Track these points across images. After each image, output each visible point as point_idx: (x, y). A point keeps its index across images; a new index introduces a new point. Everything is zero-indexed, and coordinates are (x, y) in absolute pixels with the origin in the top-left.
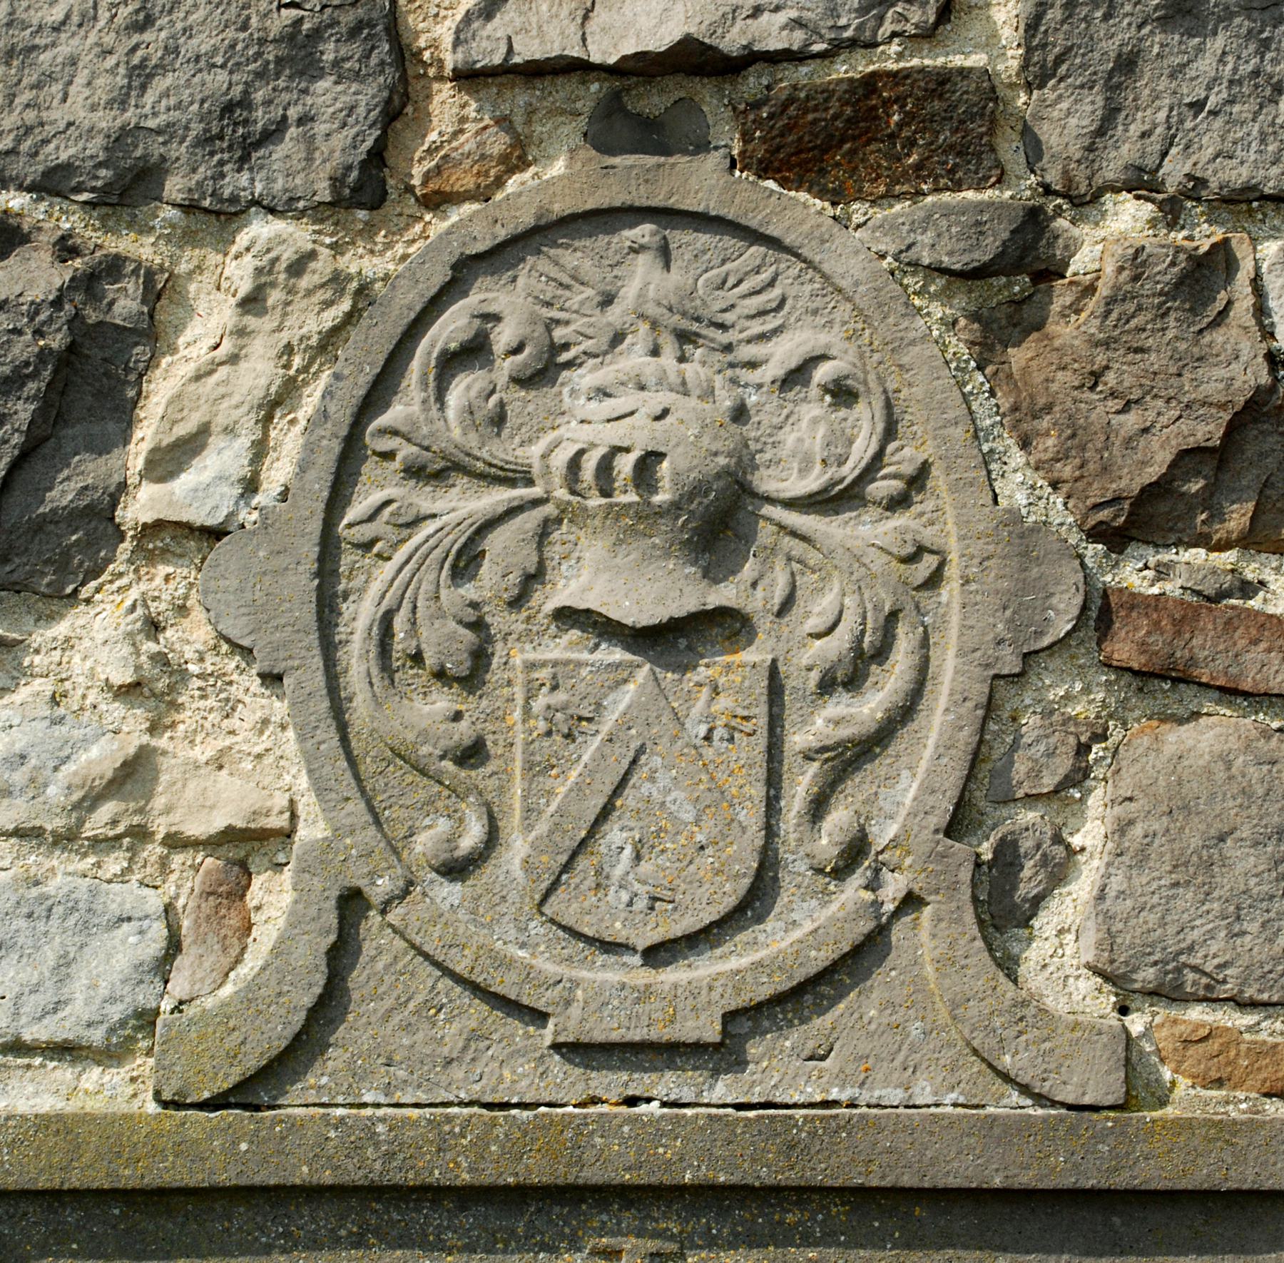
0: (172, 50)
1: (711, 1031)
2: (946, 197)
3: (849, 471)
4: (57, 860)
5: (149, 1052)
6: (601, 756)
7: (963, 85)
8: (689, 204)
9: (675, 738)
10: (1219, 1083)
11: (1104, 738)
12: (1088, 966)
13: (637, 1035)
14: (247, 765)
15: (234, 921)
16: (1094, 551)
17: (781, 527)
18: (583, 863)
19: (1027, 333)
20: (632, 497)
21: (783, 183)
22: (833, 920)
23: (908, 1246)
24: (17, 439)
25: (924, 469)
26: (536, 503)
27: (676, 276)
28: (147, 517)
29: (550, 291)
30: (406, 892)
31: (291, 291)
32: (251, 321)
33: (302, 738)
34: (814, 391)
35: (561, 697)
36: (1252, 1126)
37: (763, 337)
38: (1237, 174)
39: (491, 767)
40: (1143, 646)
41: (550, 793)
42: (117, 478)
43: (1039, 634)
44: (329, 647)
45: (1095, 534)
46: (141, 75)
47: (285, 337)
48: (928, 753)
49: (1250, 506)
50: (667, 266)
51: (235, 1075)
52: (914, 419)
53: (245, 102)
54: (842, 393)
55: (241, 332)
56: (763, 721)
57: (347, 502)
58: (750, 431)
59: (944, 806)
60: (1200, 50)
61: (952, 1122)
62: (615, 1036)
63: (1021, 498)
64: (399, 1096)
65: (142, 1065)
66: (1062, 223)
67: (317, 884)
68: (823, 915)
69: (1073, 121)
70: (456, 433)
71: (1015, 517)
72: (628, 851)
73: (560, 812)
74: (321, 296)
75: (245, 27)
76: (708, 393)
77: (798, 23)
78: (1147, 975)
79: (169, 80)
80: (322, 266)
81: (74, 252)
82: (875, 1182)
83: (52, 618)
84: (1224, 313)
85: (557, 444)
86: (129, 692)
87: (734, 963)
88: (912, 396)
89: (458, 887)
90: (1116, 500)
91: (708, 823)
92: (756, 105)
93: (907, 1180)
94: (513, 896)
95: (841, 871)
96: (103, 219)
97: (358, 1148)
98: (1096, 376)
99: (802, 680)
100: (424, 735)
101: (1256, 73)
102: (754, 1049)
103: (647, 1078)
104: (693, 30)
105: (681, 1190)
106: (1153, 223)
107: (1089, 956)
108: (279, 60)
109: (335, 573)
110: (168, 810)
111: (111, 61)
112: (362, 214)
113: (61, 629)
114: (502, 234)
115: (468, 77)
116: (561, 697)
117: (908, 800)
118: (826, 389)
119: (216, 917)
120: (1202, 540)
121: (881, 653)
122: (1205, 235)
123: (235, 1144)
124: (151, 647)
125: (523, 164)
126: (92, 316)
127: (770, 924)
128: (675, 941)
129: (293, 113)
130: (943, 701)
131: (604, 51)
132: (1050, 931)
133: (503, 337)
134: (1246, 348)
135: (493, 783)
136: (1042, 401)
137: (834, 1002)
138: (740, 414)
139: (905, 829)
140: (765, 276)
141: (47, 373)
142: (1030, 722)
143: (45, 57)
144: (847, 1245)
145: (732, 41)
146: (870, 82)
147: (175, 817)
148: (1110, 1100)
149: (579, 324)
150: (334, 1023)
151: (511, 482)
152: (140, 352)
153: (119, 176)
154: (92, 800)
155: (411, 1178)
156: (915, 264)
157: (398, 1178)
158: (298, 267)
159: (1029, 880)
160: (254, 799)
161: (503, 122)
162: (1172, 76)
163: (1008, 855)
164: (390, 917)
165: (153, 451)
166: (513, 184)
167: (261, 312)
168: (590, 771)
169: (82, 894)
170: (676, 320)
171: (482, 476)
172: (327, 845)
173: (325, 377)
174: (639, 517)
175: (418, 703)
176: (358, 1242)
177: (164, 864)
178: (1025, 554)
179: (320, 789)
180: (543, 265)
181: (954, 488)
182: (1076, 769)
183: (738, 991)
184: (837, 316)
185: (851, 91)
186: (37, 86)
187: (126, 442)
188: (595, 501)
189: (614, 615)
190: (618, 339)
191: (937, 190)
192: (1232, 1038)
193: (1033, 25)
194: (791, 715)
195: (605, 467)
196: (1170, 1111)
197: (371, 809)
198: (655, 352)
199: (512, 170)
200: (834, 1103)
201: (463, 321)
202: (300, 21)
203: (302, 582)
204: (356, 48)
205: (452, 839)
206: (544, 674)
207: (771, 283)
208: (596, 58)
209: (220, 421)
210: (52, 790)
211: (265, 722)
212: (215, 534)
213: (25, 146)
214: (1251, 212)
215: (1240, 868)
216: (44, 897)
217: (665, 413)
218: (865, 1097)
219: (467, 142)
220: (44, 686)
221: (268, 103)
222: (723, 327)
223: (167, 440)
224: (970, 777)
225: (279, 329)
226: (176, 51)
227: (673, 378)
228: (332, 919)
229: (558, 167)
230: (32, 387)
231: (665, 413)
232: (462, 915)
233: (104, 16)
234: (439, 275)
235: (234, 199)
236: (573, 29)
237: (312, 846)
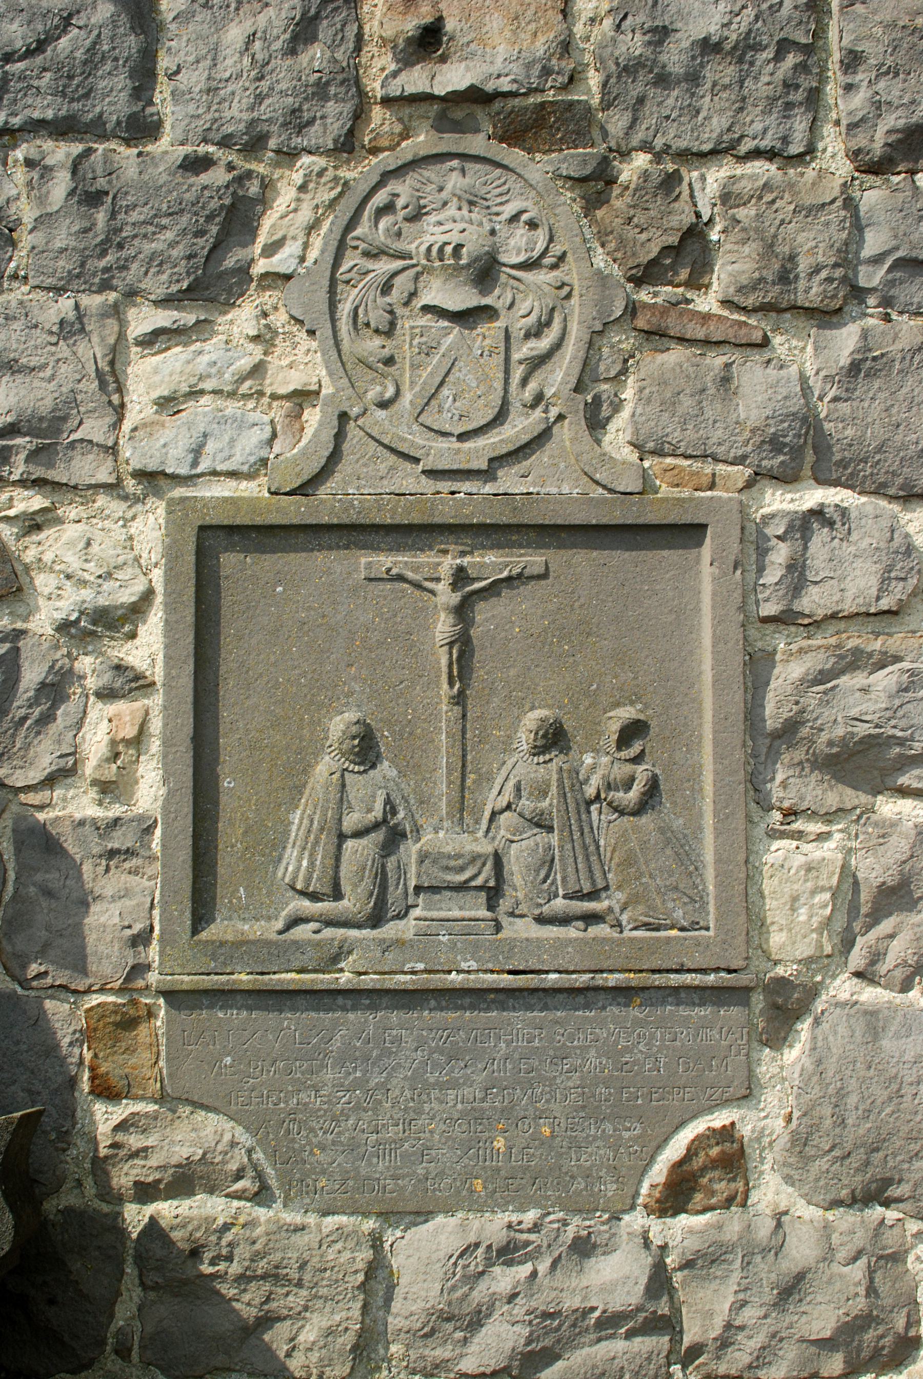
0: (271, 89)
1: (484, 466)
2: (572, 151)
3: (536, 254)
4: (229, 403)
5: (266, 475)
6: (440, 362)
7: (578, 107)
8: (472, 152)
9: (469, 355)
10: (677, 485)
11: (633, 357)
12: (628, 442)
13: (455, 467)
14: (302, 367)
15: (297, 426)
16: (630, 286)
17: (509, 275)
18: (433, 402)
19: (603, 204)
20: (452, 262)
21: (509, 145)
22: (530, 424)
23: (559, 548)
24: (212, 240)
25: (564, 254)
26: (414, 266)
27: (467, 180)
28: (263, 271)
29: (418, 186)
30: (364, 413)
31: (318, 183)
32: (302, 196)
33: (323, 355)
34: (521, 224)
35: (424, 339)
36: (691, 499)
37: (501, 204)
38: (683, 144)
39: (397, 366)
40: (649, 322)
41: (420, 376)
42: (250, 257)
43: (609, 316)
44: (333, 321)
45: (630, 279)
46: (260, 98)
47: (315, 202)
48: (567, 361)
49: (689, 270)
50: (464, 176)
51: (299, 482)
52: (559, 234)
53: (300, 110)
54: (532, 225)
55: (298, 200)
56: (502, 349)
57: (340, 266)
58: (497, 239)
59: (573, 380)
60: (668, 96)
61: (577, 500)
62: (446, 467)
63: (602, 265)
64: (362, 491)
65: (263, 480)
66: (616, 163)
67: (330, 410)
68: (526, 423)
69: (620, 123)
70: (382, 239)
71: (599, 272)
72: (451, 398)
73: (425, 383)
74: (330, 185)
75: (300, 80)
76: (480, 224)
77: (515, 81)
78: (651, 445)
79: (271, 100)
80: (330, 173)
81: (234, 168)
82: (547, 522)
83: (225, 313)
84: (678, 196)
85: (422, 243)
86: (256, 339)
87: (492, 440)
88: (560, 226)
89: (384, 412)
90: (638, 266)
91: (482, 387)
92: (498, 114)
93: (559, 522)
94: (406, 416)
95: (533, 406)
96: (245, 156)
97: (346, 510)
98: (630, 219)
99: (517, 333)
100: (371, 354)
101: (690, 105)
102: (500, 473)
103: (459, 484)
104: (474, 82)
105: (472, 526)
106: (651, 162)
107: (628, 438)
108: (313, 93)
109: (335, 293)
110: (271, 384)
111: (248, 93)
112: (345, 155)
113: (229, 317)
114: (400, 163)
115: (387, 101)
116: (424, 339)
117: (559, 379)
118: (526, 223)
119: (290, 425)
120: (670, 283)
121: (548, 324)
122: (671, 167)
123: (300, 508)
124: (263, 322)
125: (407, 137)
126: (241, 193)
127: (506, 426)
128: (469, 432)
129: (318, 115)
130: (572, 342)
131: (440, 90)
132: (613, 430)
133: (400, 203)
134: (687, 209)
135: (398, 372)
136: (609, 230)
137: (531, 455)
138: (493, 232)
139: (558, 390)
140: (502, 180)
141: (223, 214)
142: (605, 350)
143: (222, 92)
144: (536, 548)
145: (490, 87)
146: (543, 105)
147: (274, 387)
148: (637, 490)
149: (430, 198)
150: (336, 464)
151: (404, 258)
152: (259, 208)
153: (251, 139)
154: (242, 380)
155: (368, 521)
156: (560, 176)
157: (363, 521)
158: (320, 174)
159: (605, 411)
160: (305, 379)
161: (400, 120)
162: (658, 106)
163: (597, 400)
164: (359, 423)
165: (265, 245)
166: (404, 144)
167: (306, 192)
168: (436, 367)
169: (239, 415)
170: (467, 196)
171: (393, 256)
172: (333, 395)
173: (331, 217)
174: (455, 270)
175: (368, 342)
176: (347, 547)
177: (270, 405)
178: (604, 286)
179: (330, 374)
180: (416, 176)
181: (575, 261)
182: (623, 368)
183: (494, 450)
184: (530, 196)
185: (535, 108)
186: (219, 103)
187: (254, 243)
188: (437, 264)
189: (445, 307)
190: (445, 204)
191: (568, 148)
192: (683, 469)
193: (605, 85)
194: (514, 347)
195: (441, 250)
196: (659, 495)
197: (350, 382)
198: (460, 209)
199: (404, 139)
200: (531, 493)
201: (385, 196)
202: (321, 78)
203: (322, 295)
204: (343, 89)
205: (382, 394)
206: (417, 331)
207: (505, 183)
208: (436, 93)
209: (290, 234)
210: (226, 376)
211: (309, 350)
212: (288, 277)
213: (214, 127)
214: (687, 160)
215: (686, 404)
216: (224, 416)
217: (464, 231)
218: (543, 491)
219: (386, 128)
220: (223, 338)
221: (309, 110)
222: (486, 199)
223: (270, 241)
224: (583, 371)
225: (313, 199)
226: (273, 89)
227: (467, 218)
228: (336, 423)
229: (422, 138)
230: (217, 220)
231: (464, 231)
232: (386, 422)
233: (245, 75)
234: (375, 178)
235: (295, 148)
236: (427, 83)
237: (327, 396)
